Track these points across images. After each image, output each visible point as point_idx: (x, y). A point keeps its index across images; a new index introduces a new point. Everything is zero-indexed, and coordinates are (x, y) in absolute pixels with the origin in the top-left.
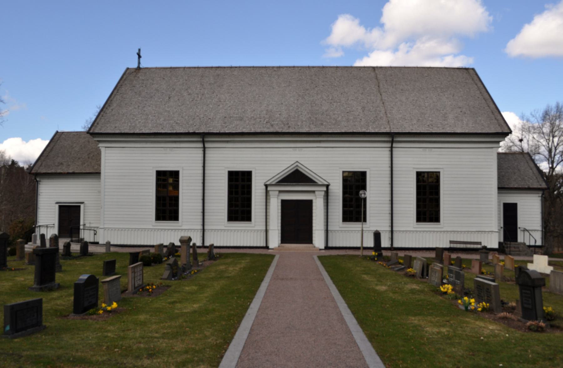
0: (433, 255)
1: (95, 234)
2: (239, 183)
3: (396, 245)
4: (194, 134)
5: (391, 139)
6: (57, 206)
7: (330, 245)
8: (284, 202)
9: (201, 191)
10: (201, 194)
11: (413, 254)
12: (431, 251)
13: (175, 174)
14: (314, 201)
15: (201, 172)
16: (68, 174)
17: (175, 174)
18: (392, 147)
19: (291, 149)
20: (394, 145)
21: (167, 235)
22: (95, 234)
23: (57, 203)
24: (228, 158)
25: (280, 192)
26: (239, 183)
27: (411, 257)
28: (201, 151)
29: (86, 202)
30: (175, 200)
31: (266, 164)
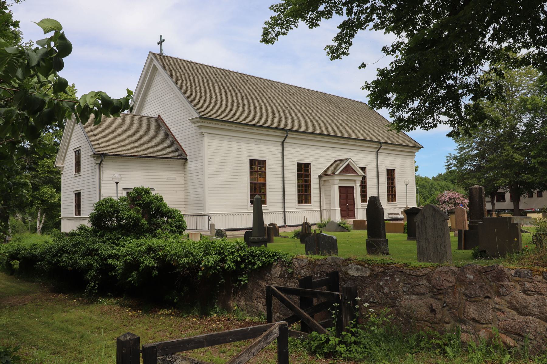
2: (304, 170)
5: (285, 135)
8: (339, 187)
10: (281, 182)
13: (262, 163)
15: (281, 162)
25: (341, 180)
26: (304, 170)
31: (320, 158)
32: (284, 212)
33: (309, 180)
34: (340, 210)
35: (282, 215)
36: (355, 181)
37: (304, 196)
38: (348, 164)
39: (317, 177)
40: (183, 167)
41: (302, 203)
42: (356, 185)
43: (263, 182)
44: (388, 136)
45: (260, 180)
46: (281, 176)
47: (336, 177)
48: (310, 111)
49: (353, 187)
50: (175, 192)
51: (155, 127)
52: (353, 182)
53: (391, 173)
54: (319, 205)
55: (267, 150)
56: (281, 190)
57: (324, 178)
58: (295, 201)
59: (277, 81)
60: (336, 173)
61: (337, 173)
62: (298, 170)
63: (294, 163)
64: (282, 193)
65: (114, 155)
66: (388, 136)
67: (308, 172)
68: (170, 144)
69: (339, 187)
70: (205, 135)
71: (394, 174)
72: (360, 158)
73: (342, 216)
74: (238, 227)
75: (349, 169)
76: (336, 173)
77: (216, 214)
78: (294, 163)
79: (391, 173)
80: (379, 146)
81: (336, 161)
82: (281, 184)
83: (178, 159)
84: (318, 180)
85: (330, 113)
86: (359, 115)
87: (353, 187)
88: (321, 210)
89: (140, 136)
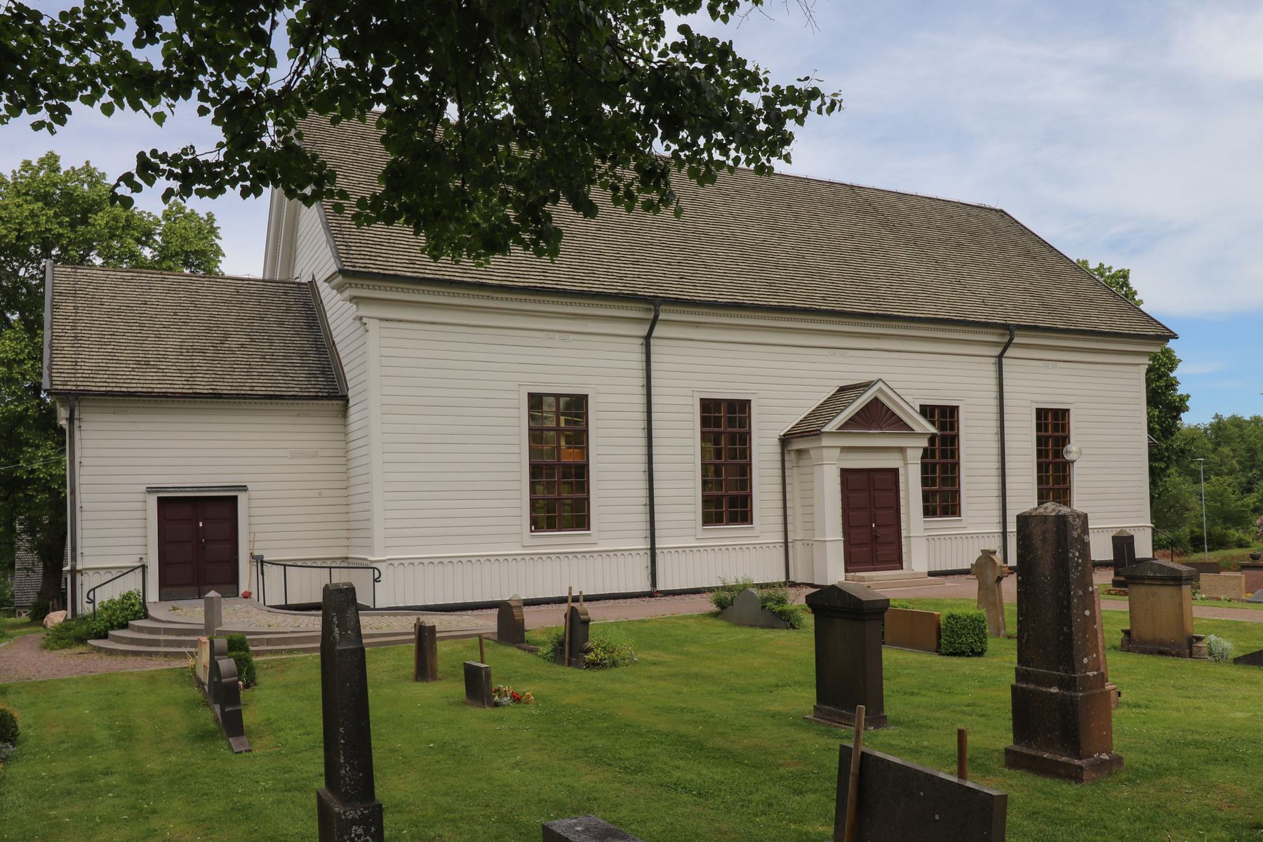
0: (488, 623)
1: (375, 580)
2: (725, 424)
3: (660, 587)
4: (633, 298)
5: (651, 316)
6: (152, 501)
7: (792, 578)
8: (844, 472)
9: (643, 450)
10: (644, 459)
11: (430, 620)
12: (485, 612)
13: (577, 405)
14: (901, 472)
15: (642, 399)
16: (149, 395)
17: (577, 405)
18: (648, 338)
19: (543, 334)
20: (1009, 352)
21: (551, 570)
22: (375, 580)
23: (151, 490)
24: (704, 362)
25: (845, 449)
26: (725, 424)
27: (432, 629)
28: (637, 348)
29: (250, 486)
30: (579, 474)
31: (784, 379)
32: (653, 550)
33: (746, 453)
34: (841, 546)
35: (646, 560)
36: (902, 450)
37: (727, 501)
38: (876, 399)
39: (776, 441)
40: (341, 421)
41: (934, 514)
42: (906, 464)
43: (578, 460)
44: (1045, 305)
45: (569, 457)
46: (643, 442)
47: (826, 442)
48: (775, 240)
49: (896, 471)
50: (315, 493)
51: (288, 310)
52: (898, 456)
53: (1053, 427)
54: (780, 527)
55: (592, 361)
56: (644, 485)
57: (797, 445)
58: (692, 516)
59: (998, 208)
60: (826, 429)
61: (832, 427)
62: (1039, 428)
63: (689, 401)
64: (645, 493)
65: (107, 394)
66: (1045, 305)
67: (1064, 430)
68: (312, 354)
69: (844, 472)
70: (373, 325)
71: (585, 415)
72: (915, 375)
73: (851, 563)
74: (960, 567)
75: (877, 416)
76: (826, 429)
77: (390, 562)
78: (689, 401)
79: (1053, 427)
80: (1006, 340)
81: (842, 389)
82: (644, 467)
83: (316, 398)
84: (778, 449)
85: (849, 244)
86: (959, 245)
87: (896, 471)
88: (653, 550)
89: (226, 336)
